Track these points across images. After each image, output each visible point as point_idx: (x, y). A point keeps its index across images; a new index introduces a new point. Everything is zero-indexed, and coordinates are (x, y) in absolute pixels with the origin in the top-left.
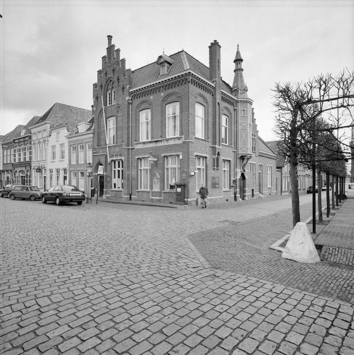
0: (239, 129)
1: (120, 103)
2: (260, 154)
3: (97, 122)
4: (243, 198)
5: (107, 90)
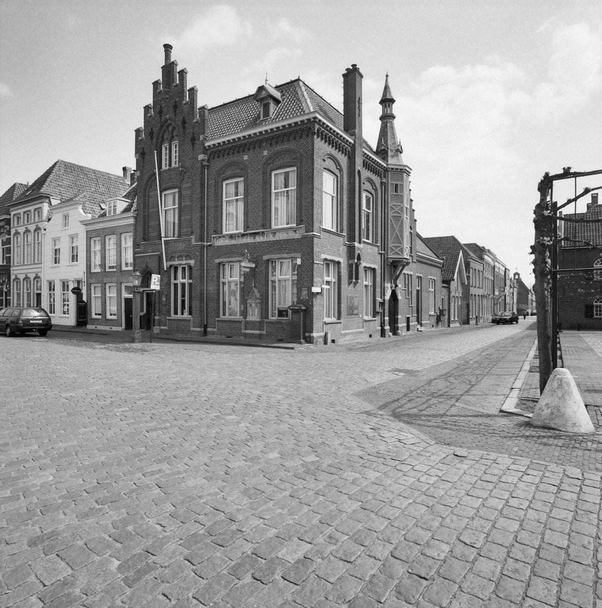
0: (390, 217)
1: (187, 164)
3: (142, 197)
4: (395, 331)
5: (163, 140)
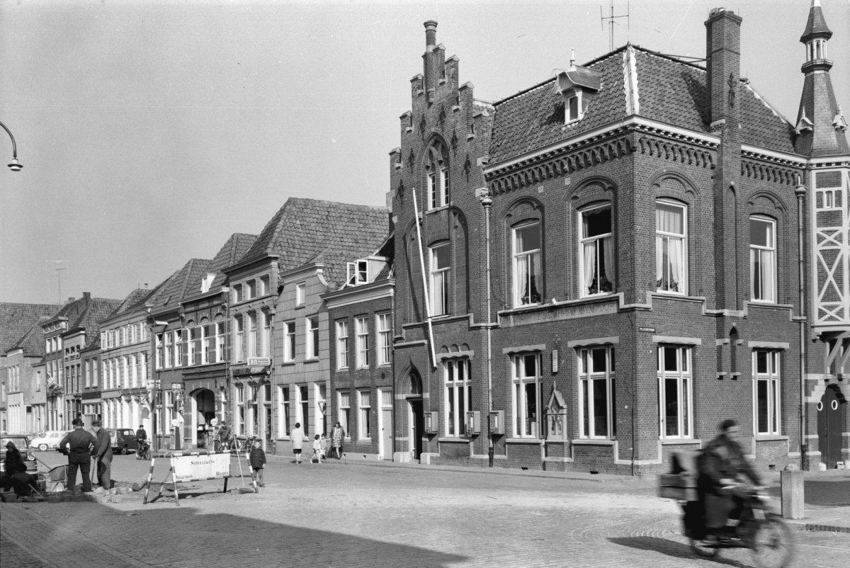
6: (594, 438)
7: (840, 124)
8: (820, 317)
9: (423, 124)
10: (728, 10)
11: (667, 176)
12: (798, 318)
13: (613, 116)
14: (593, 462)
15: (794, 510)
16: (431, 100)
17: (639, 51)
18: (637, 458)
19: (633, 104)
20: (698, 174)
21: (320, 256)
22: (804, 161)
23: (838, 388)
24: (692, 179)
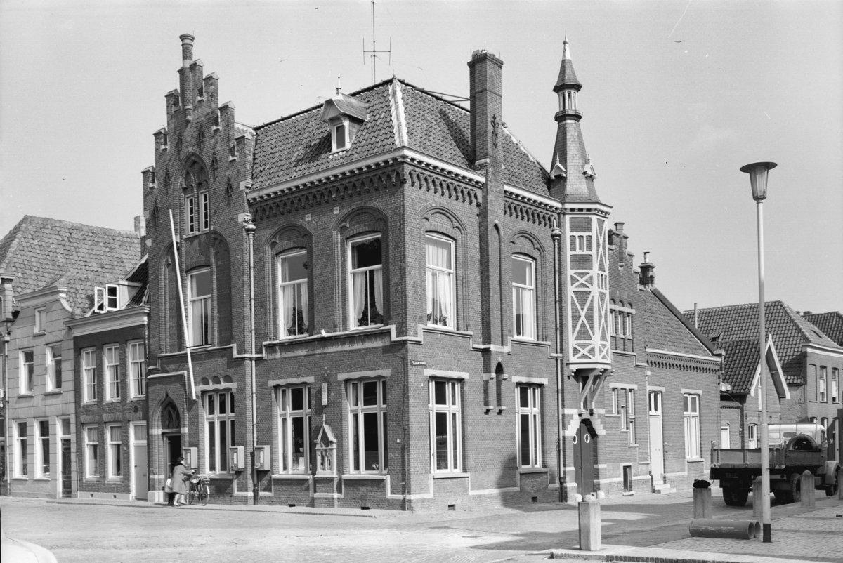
2: (654, 359)
6: (364, 473)
7: (589, 173)
8: (574, 354)
9: (179, 143)
10: (490, 52)
11: (437, 210)
12: (555, 355)
13: (382, 148)
14: (364, 498)
15: (592, 542)
16: (189, 118)
17: (404, 86)
18: (409, 493)
19: (402, 136)
20: (466, 212)
21: (62, 280)
22: (559, 205)
23: (590, 422)
24: (459, 215)
